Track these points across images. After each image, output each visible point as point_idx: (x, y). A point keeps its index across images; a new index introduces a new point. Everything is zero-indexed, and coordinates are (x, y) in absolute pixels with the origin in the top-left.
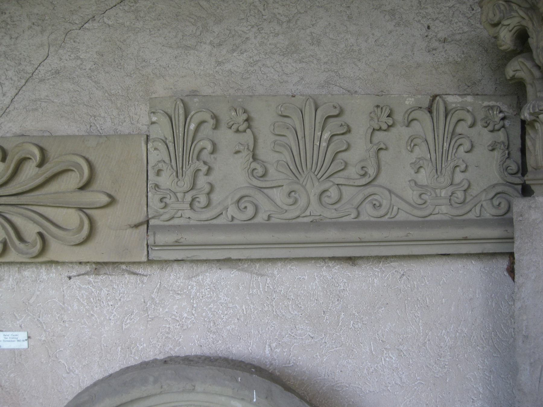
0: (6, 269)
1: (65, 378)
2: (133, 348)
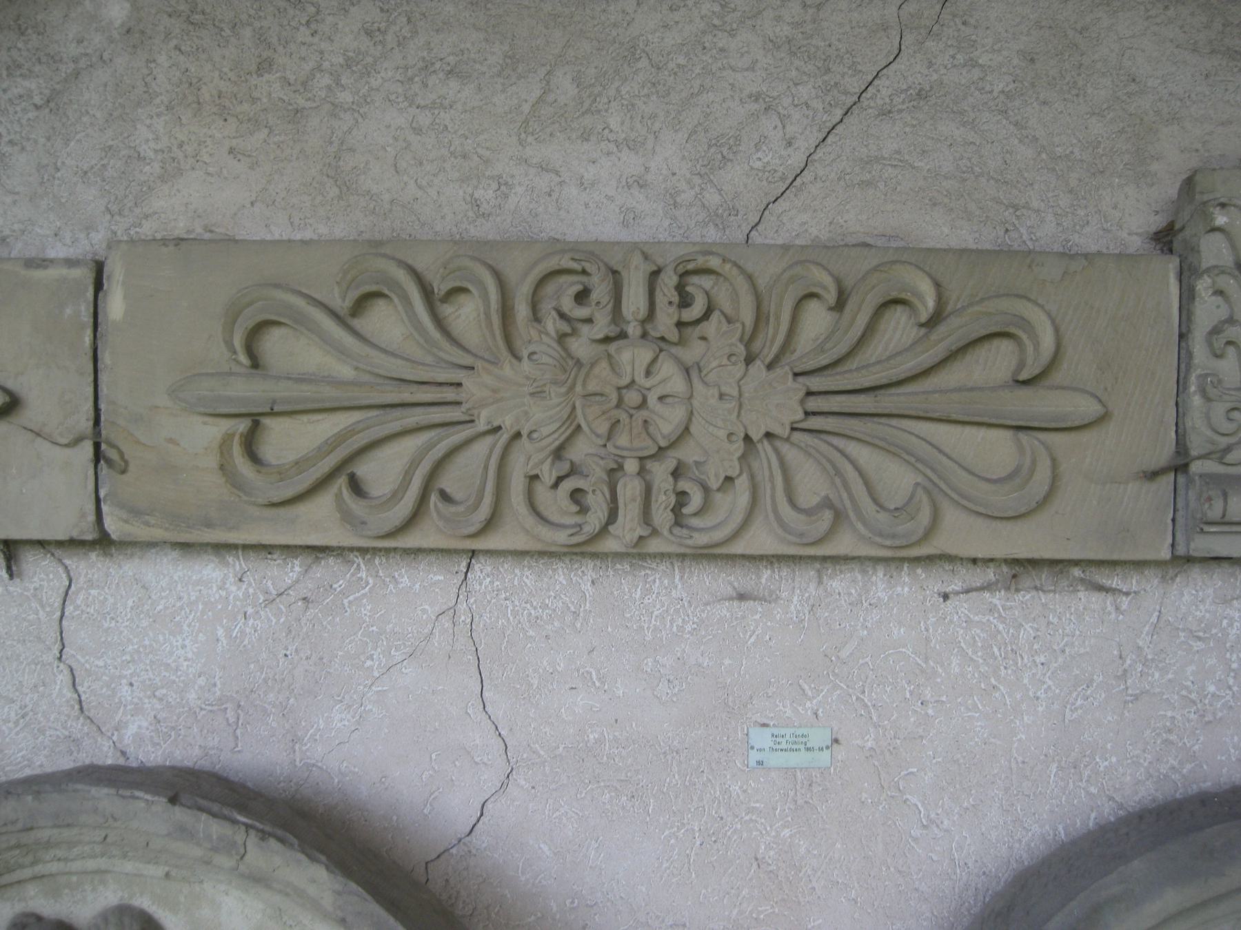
0: (785, 572)
1: (915, 840)
2: (1086, 766)
